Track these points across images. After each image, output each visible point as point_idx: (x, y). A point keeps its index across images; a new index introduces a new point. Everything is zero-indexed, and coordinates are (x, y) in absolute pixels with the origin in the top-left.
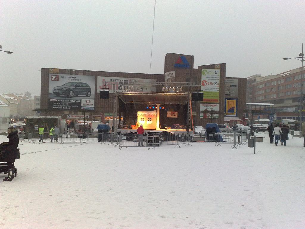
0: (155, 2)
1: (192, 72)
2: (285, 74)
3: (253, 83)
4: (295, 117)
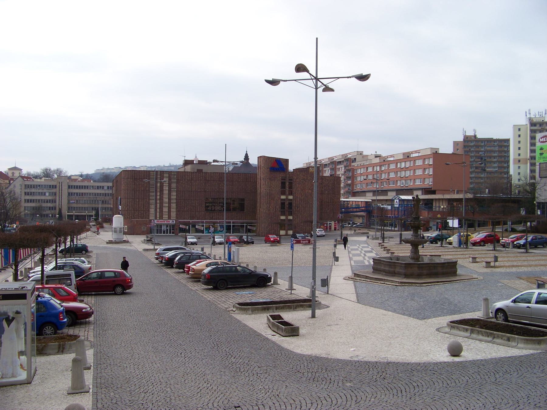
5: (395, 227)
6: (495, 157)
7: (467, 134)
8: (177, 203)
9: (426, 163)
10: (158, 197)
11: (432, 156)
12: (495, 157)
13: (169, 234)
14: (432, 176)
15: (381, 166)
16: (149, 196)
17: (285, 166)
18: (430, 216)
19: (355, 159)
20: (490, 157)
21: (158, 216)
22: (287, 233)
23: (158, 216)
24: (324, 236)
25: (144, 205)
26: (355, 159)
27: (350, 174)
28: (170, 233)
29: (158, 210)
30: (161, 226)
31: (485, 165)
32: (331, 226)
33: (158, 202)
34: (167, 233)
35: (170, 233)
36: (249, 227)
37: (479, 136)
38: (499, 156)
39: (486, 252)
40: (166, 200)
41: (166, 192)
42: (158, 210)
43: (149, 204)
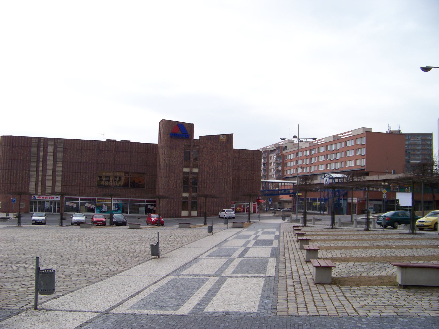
0: (153, 284)
1: (193, 144)
2: (344, 135)
3: (284, 150)
4: (111, 174)
5: (325, 210)
6: (418, 150)
7: (392, 130)
8: (63, 177)
9: (359, 143)
10: (41, 169)
11: (365, 135)
12: (418, 150)
13: (53, 213)
14: (365, 157)
15: (310, 150)
16: (30, 166)
17: (189, 133)
18: (366, 197)
19: (286, 147)
20: (414, 150)
21: (39, 191)
22: (190, 213)
23: (39, 191)
24: (234, 218)
25: (22, 177)
26: (286, 147)
27: (281, 161)
28: (55, 211)
29: (40, 184)
30: (43, 203)
31: (409, 157)
32: (249, 208)
33: (40, 174)
34: (51, 211)
35: (55, 211)
36: (149, 207)
37: (403, 132)
38: (422, 149)
39: (357, 233)
40: (50, 172)
41: (50, 162)
42: (40, 184)
43: (29, 176)
